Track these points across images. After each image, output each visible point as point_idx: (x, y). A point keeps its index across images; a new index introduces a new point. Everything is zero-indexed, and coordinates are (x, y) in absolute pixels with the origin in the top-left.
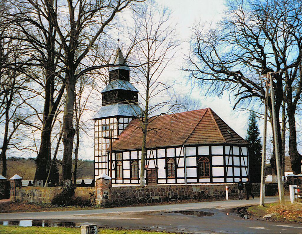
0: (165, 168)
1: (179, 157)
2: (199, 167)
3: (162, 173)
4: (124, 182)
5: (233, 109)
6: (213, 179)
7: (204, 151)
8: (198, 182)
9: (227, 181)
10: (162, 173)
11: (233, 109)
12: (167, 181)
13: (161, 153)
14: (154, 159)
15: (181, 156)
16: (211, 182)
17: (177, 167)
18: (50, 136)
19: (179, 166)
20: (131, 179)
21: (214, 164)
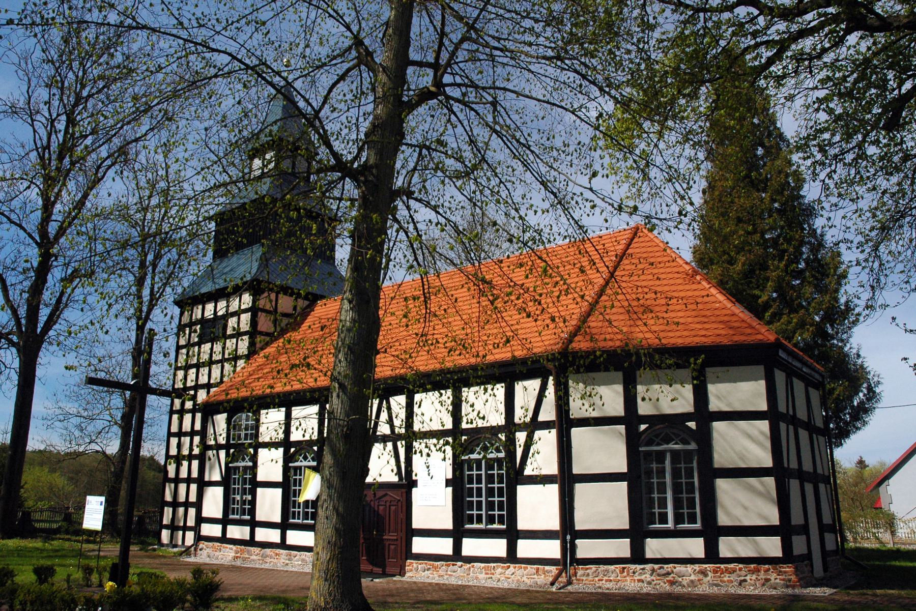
0: (448, 483)
1: (534, 425)
2: (638, 478)
3: (432, 504)
4: (465, 552)
5: (91, 381)
6: (248, 528)
7: (670, 398)
8: (638, 556)
9: (649, 555)
10: (432, 504)
11: (91, 381)
12: (283, 537)
13: (432, 410)
14: (393, 438)
15: (541, 418)
16: (712, 555)
17: (256, 484)
18: (35, 364)
19: (528, 471)
20: (458, 534)
21: (722, 457)
